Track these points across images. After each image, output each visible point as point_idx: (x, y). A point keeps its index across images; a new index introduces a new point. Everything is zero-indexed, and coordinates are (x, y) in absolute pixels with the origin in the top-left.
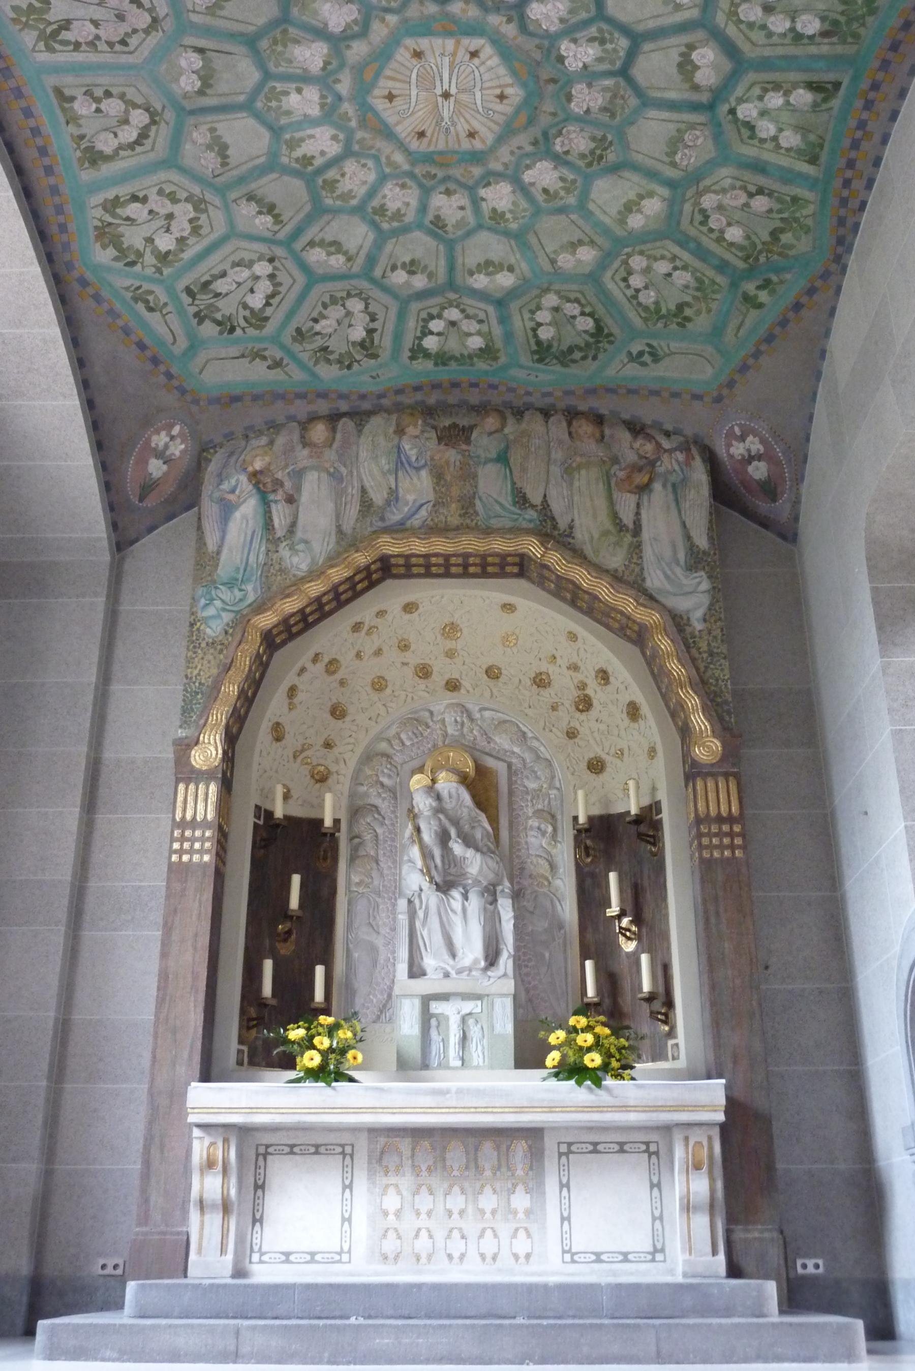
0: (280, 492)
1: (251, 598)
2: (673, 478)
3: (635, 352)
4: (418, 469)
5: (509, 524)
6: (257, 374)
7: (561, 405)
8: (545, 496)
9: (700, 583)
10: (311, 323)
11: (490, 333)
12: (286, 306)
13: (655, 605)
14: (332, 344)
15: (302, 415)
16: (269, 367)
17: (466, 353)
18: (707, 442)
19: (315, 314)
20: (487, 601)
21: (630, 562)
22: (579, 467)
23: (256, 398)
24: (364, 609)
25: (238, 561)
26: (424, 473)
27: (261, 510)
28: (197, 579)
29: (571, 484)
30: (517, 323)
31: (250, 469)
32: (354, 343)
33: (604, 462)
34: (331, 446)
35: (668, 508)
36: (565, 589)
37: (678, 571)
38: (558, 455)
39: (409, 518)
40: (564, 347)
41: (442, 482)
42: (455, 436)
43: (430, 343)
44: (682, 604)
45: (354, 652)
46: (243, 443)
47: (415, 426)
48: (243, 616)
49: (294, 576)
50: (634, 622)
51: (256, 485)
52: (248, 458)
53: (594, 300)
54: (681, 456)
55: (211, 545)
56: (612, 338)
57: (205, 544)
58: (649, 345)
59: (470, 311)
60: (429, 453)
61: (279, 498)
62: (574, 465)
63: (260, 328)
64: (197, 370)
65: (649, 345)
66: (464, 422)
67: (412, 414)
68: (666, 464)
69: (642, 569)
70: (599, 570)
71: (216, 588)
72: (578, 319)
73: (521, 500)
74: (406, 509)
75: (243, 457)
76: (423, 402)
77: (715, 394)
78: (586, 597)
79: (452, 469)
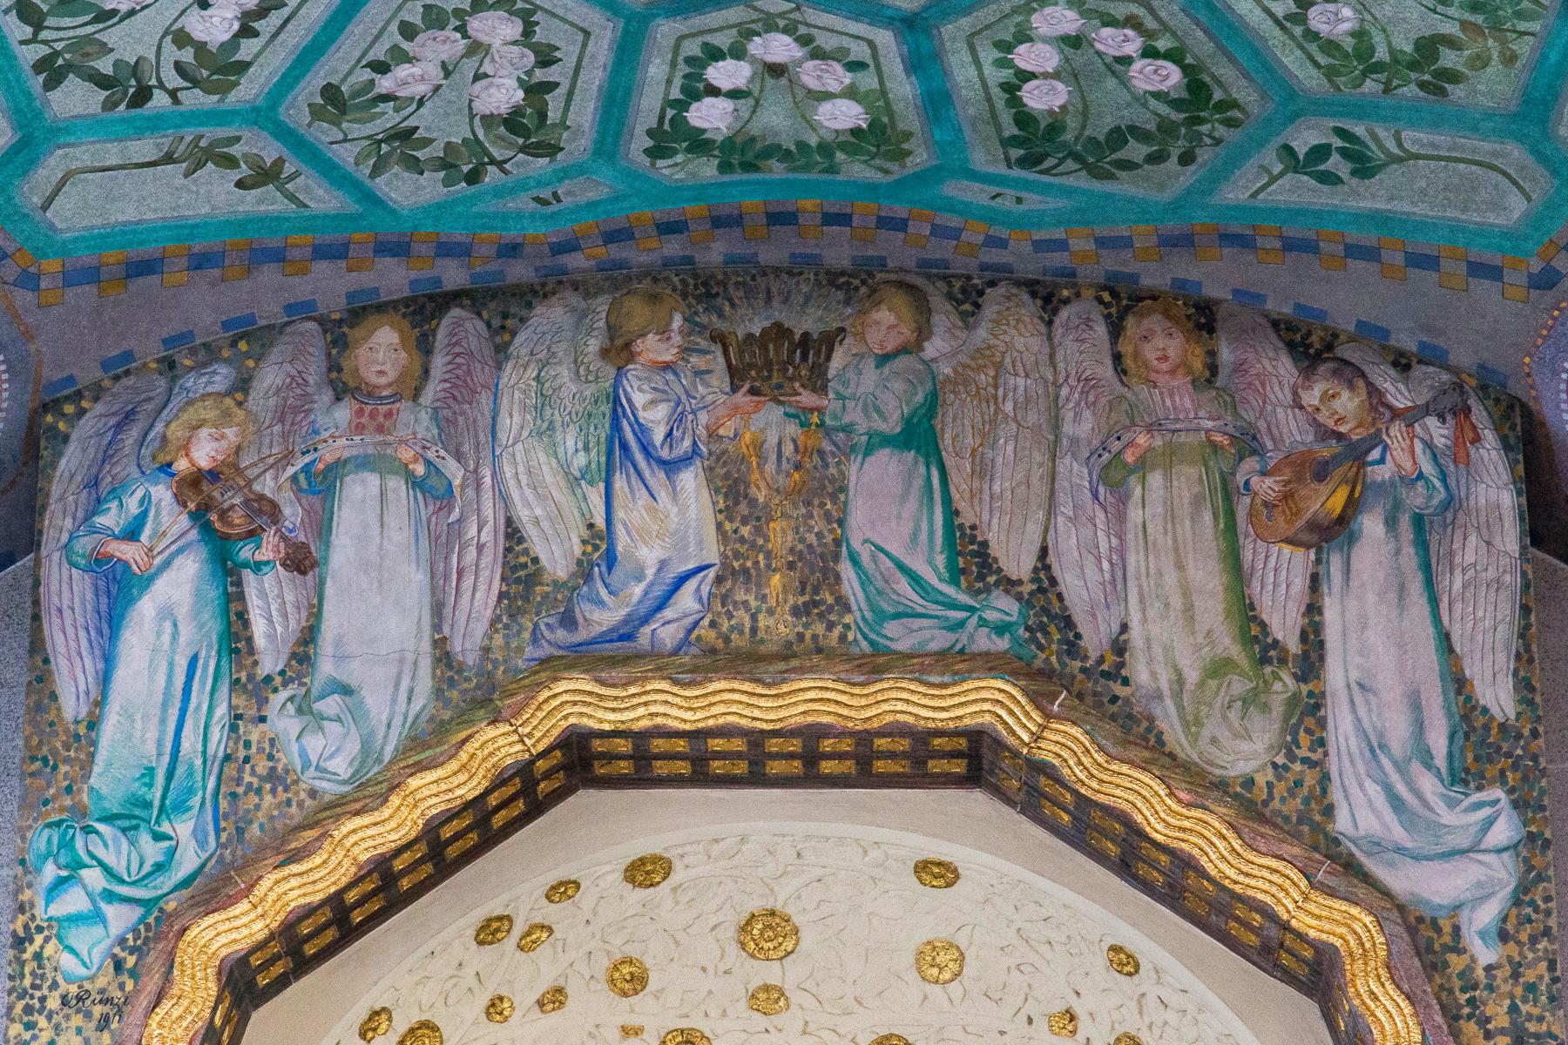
0: (270, 538)
1: (188, 861)
2: (1416, 499)
3: (1302, 151)
4: (671, 467)
5: (939, 640)
6: (214, 197)
7: (1090, 272)
8: (1044, 552)
9: (1489, 823)
10: (368, 74)
11: (883, 93)
12: (295, 37)
13: (1361, 891)
14: (423, 120)
15: (333, 302)
16: (240, 184)
17: (813, 141)
18: (1516, 388)
19: (379, 52)
20: (874, 854)
21: (1291, 756)
22: (1143, 466)
23: (201, 261)
24: (511, 877)
25: (150, 748)
26: (690, 479)
27: (213, 593)
28: (33, 803)
29: (1121, 517)
30: (962, 72)
31: (182, 465)
32: (489, 120)
33: (1215, 447)
34: (416, 395)
35: (1402, 590)
36: (1104, 833)
37: (1429, 785)
38: (1081, 426)
39: (645, 620)
40: (1100, 129)
41: (743, 508)
42: (780, 364)
43: (711, 116)
44: (1433, 885)
45: (483, 1000)
46: (162, 383)
47: (664, 332)
48: (164, 917)
49: (313, 793)
50: (1301, 936)
51: (199, 516)
52: (176, 431)
53: (1181, 22)
54: (1439, 432)
55: (71, 706)
56: (1236, 114)
57: (54, 697)
58: (1341, 133)
59: (826, 42)
60: (703, 417)
61: (265, 554)
62: (1129, 457)
63: (223, 89)
64: (37, 200)
65: (1341, 133)
66: (808, 322)
67: (654, 298)
68: (1402, 455)
69: (1325, 778)
70: (1200, 783)
71: (88, 830)
72: (1138, 65)
73: (972, 560)
74: (638, 590)
75: (159, 427)
76: (689, 260)
77: (1536, 266)
78: (1163, 858)
79: (770, 467)
